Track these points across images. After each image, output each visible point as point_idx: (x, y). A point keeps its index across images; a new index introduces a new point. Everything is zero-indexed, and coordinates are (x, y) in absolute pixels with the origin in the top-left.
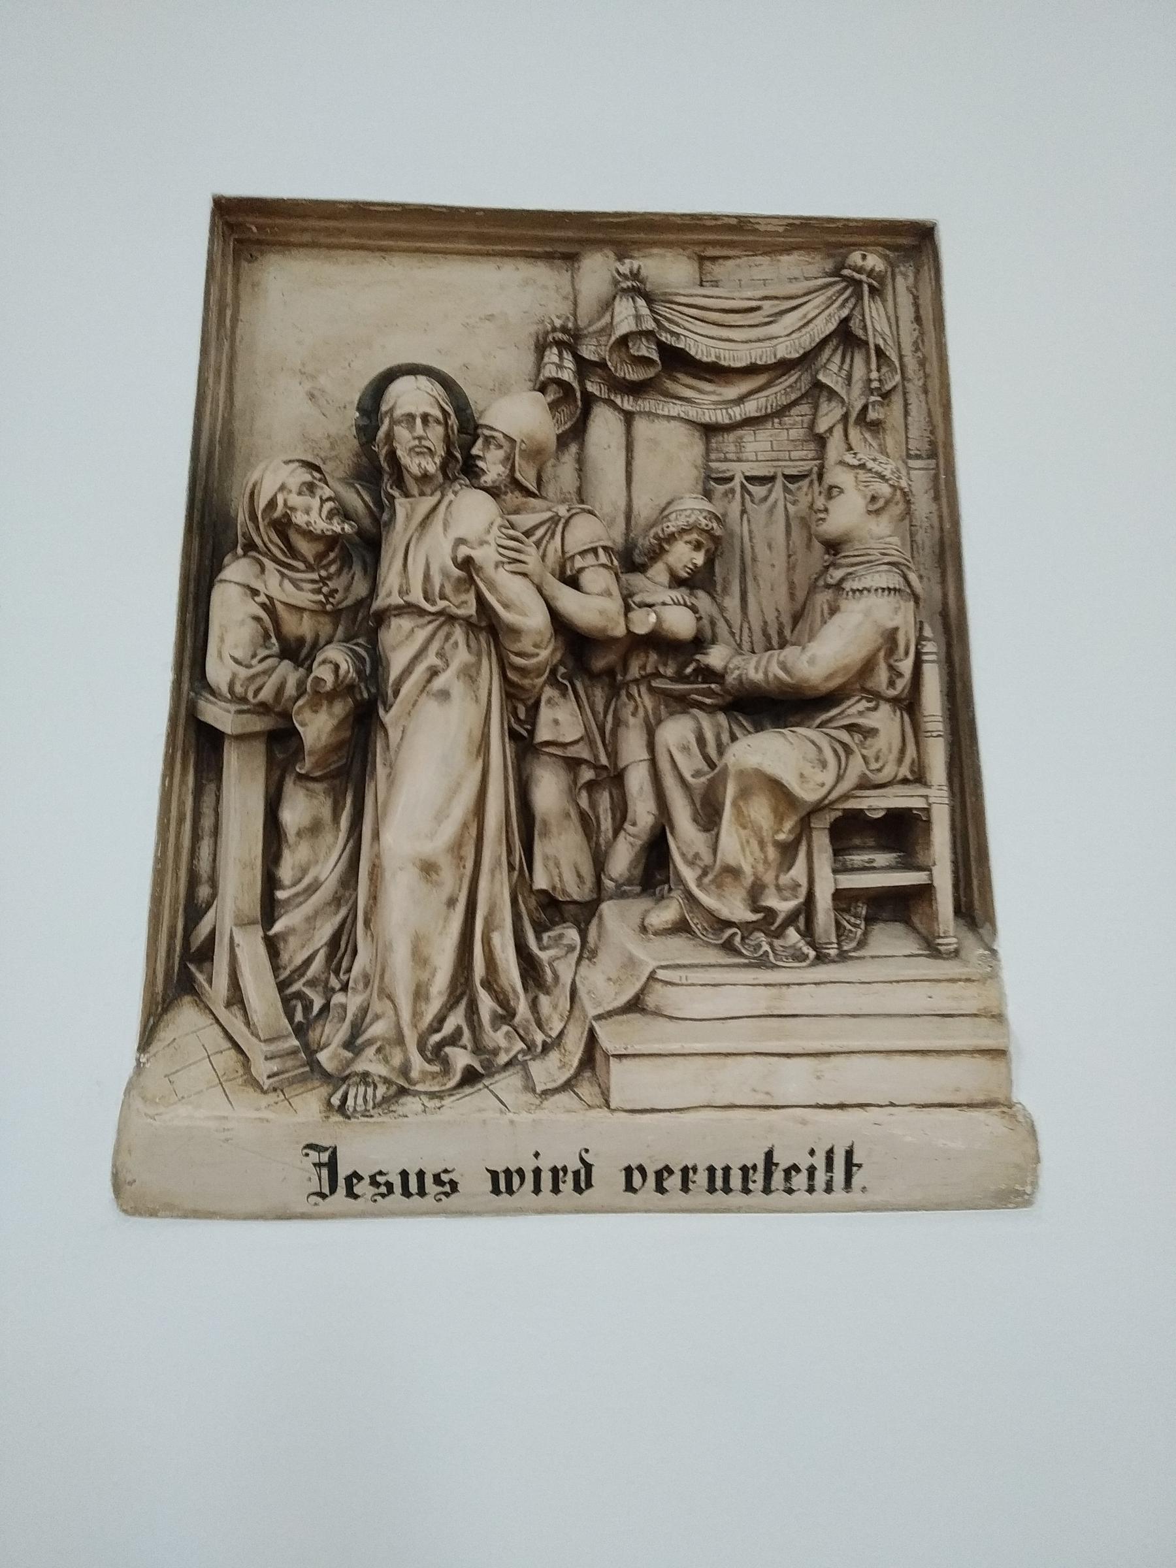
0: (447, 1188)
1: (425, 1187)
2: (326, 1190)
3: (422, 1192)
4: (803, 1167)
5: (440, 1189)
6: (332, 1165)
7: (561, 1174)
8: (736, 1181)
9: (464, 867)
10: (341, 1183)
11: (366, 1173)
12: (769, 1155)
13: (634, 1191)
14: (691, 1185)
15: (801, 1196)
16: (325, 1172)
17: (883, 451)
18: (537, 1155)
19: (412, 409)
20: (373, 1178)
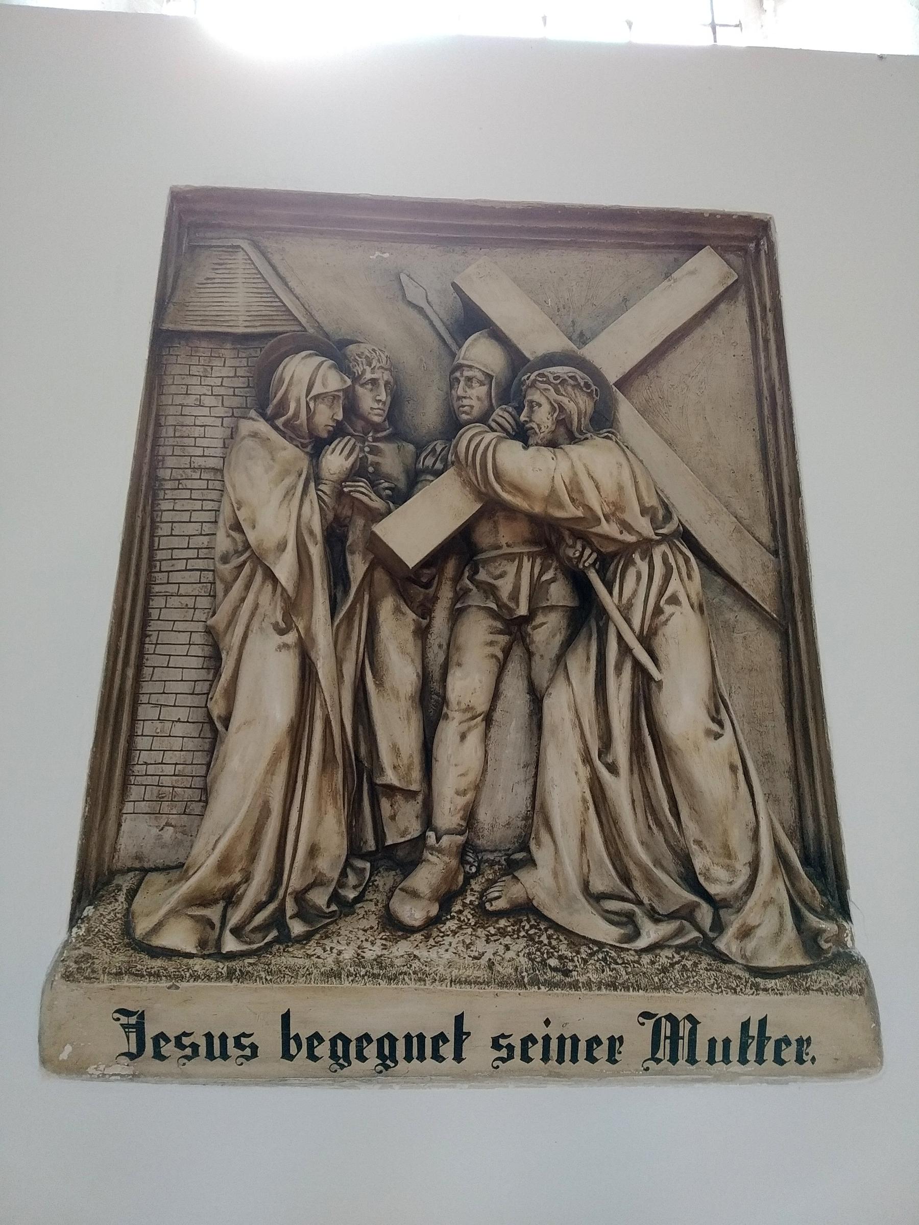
0: (188, 1051)
1: (221, 1049)
2: (134, 1050)
3: (224, 1056)
4: (539, 1037)
5: (241, 1053)
6: (139, 1028)
7: (618, 1044)
11: (171, 1035)
12: (459, 1020)
13: (291, 1058)
14: (617, 1057)
15: (735, 1067)
16: (133, 1036)
18: (547, 1022)
20: (178, 1039)
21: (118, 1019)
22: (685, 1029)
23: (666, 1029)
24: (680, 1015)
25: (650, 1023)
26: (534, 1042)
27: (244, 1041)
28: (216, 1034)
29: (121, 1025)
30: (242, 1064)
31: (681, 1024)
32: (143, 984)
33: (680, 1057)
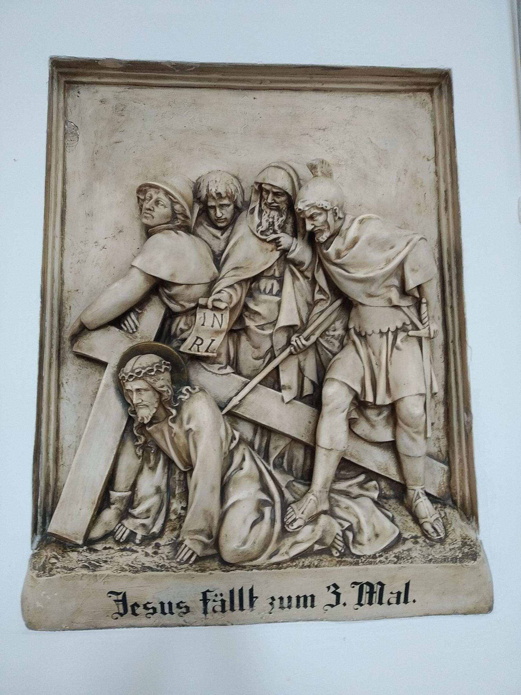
0: (184, 610)
2: (122, 611)
6: (124, 601)
8: (294, 601)
9: (302, 296)
10: (129, 609)
12: (407, 585)
17: (278, 219)
19: (222, 190)
21: (110, 597)
22: (377, 588)
23: (366, 588)
24: (374, 582)
25: (357, 587)
26: (138, 606)
27: (181, 605)
28: (166, 602)
29: (409, 582)
30: (117, 618)
31: (375, 586)
32: (262, 571)
33: (374, 601)
